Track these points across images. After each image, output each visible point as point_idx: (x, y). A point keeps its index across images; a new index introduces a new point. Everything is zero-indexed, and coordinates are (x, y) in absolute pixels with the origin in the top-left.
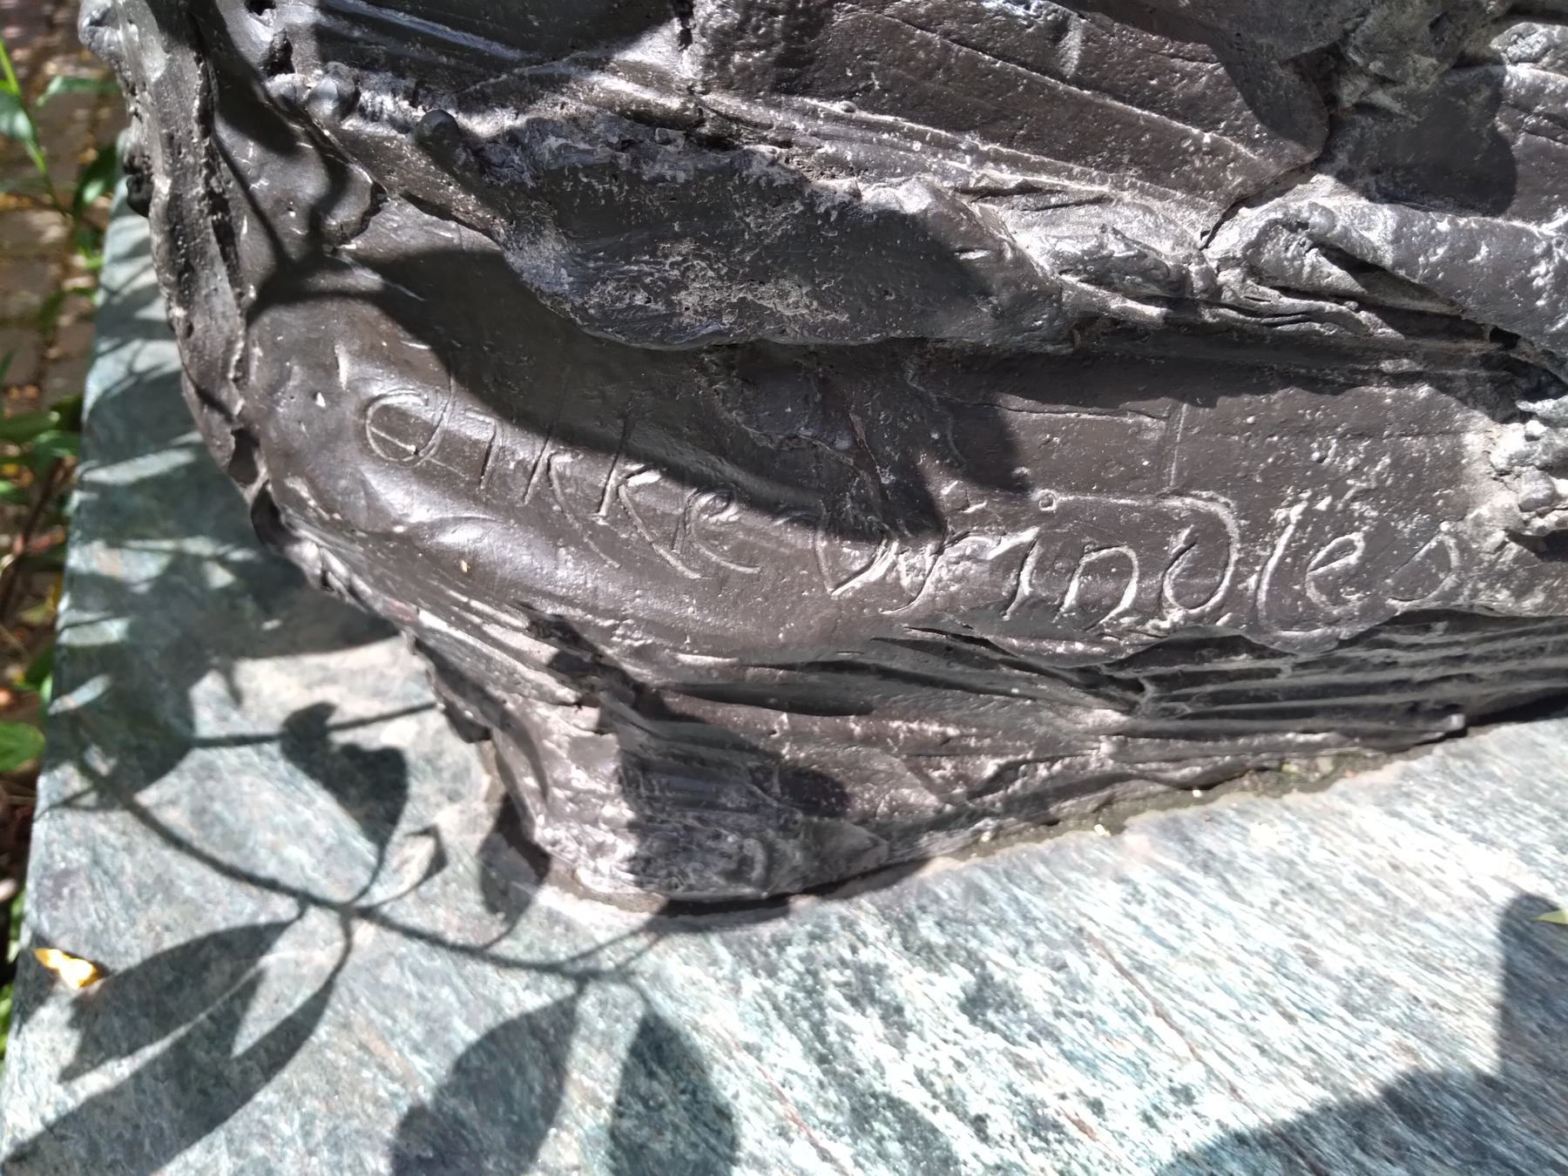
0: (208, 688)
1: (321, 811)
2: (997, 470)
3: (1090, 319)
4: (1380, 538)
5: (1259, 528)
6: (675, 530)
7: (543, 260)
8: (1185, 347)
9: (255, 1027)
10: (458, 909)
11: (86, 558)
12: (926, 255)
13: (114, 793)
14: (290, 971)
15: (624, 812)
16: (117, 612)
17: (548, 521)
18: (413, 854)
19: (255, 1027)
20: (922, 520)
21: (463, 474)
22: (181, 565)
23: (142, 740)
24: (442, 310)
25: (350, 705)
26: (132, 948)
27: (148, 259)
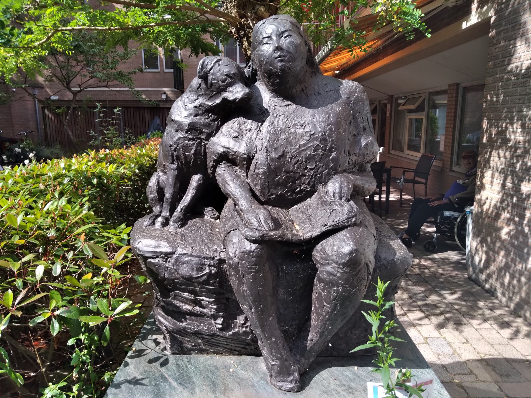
0: (150, 336)
1: (154, 344)
2: (186, 319)
3: (186, 311)
4: (208, 327)
5: (200, 325)
6: (171, 321)
7: (165, 306)
8: (191, 314)
9: (144, 354)
10: (159, 351)
11: (145, 326)
12: (178, 307)
13: (141, 341)
14: (146, 352)
15: (170, 343)
16: (91, 145)
17: (166, 319)
18: (158, 348)
19: (144, 354)
20: (182, 322)
21: (162, 316)
22: (152, 328)
23: (145, 338)
24: (163, 308)
25: (159, 339)
26: (138, 349)
27: (524, 269)
